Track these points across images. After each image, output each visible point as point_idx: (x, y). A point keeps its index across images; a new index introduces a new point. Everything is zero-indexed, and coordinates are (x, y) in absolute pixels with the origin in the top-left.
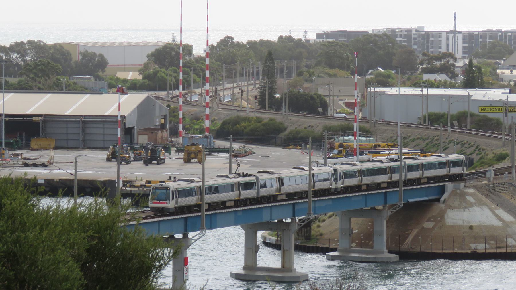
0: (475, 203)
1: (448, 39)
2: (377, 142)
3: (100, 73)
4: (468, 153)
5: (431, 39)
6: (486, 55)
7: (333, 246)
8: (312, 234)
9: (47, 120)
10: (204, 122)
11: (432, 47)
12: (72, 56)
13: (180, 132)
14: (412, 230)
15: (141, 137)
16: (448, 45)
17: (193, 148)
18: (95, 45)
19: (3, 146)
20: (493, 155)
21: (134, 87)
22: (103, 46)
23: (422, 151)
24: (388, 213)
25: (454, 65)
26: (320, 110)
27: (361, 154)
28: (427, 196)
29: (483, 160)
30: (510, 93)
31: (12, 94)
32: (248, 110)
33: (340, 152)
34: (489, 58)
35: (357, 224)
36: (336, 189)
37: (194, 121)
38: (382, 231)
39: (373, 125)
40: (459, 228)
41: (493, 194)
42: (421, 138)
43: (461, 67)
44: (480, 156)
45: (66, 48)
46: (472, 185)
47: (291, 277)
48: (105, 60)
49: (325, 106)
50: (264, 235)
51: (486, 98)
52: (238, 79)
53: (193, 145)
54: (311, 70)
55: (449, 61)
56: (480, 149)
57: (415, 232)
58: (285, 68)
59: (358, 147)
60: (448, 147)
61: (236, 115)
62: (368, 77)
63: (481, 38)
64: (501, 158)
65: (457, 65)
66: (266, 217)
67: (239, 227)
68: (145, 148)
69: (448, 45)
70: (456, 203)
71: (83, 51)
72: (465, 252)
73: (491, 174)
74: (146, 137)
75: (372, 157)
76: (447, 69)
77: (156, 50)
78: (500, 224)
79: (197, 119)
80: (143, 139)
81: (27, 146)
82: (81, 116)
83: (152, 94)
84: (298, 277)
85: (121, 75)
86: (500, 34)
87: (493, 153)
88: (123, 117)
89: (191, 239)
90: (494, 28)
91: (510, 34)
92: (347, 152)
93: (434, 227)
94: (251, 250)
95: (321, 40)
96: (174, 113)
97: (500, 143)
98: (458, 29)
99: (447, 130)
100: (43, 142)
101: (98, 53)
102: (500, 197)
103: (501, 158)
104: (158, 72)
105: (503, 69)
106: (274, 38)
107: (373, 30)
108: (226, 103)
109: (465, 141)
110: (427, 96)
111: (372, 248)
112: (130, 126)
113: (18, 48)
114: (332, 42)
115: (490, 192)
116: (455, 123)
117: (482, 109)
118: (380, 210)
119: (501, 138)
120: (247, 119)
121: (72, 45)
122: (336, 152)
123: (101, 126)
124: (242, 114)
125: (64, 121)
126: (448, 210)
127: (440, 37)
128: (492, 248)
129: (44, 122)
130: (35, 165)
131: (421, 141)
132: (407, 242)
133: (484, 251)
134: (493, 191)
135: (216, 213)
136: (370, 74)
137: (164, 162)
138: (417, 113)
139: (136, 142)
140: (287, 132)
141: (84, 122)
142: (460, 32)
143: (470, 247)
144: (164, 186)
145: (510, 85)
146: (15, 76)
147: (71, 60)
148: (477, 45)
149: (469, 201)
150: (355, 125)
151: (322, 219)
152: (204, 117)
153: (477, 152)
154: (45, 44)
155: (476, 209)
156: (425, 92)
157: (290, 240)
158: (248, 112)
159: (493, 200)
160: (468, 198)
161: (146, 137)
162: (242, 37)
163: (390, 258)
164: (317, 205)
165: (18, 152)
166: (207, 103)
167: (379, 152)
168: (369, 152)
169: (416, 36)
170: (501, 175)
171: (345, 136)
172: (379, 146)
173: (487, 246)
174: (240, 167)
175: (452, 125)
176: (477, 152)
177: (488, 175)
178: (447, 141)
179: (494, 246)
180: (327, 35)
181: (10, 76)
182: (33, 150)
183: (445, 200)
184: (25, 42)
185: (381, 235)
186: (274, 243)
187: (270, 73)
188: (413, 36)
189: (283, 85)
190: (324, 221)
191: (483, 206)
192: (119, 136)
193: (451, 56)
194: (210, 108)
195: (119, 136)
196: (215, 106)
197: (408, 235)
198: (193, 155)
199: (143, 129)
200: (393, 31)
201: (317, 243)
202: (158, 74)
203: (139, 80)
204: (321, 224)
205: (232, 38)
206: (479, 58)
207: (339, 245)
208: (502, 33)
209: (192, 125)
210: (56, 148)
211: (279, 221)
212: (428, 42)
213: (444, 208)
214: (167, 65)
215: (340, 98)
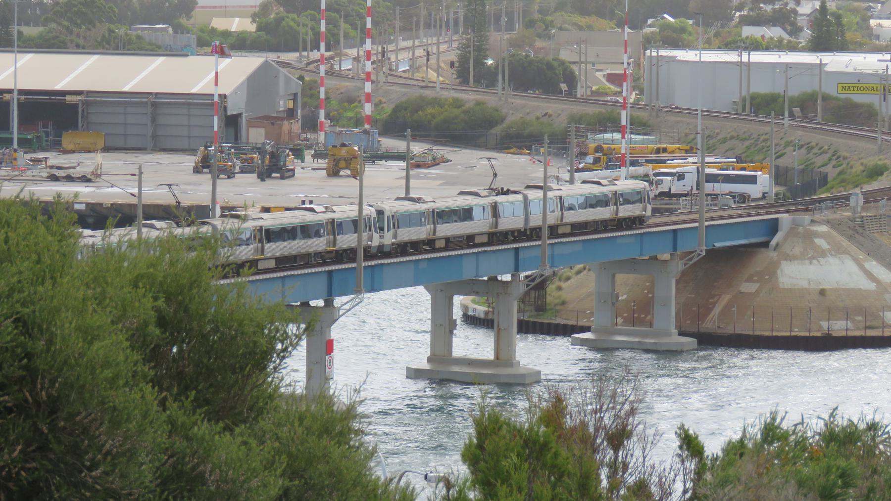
3: (183, 21)
4: (819, 164)
7: (583, 322)
8: (548, 301)
10: (362, 107)
13: (322, 122)
14: (720, 296)
15: (252, 130)
19: (15, 146)
20: (862, 168)
21: (241, 44)
23: (739, 160)
24: (679, 266)
25: (795, 12)
26: (564, 87)
27: (634, 163)
28: (745, 238)
29: (843, 176)
31: (96, 57)
32: (438, 86)
33: (597, 161)
35: (626, 285)
36: (381, 247)
37: (346, 104)
39: (654, 114)
41: (862, 235)
42: (737, 137)
43: (808, 15)
44: (840, 169)
47: (509, 376)
49: (571, 80)
50: (464, 302)
51: (850, 69)
53: (343, 145)
54: (549, 18)
57: (725, 299)
58: (503, 15)
59: (628, 152)
62: (647, 30)
64: (876, 173)
65: (800, 10)
66: (468, 271)
67: (421, 289)
68: (260, 150)
70: (798, 250)
73: (857, 200)
74: (262, 131)
75: (653, 170)
78: (872, 286)
79: (350, 100)
80: (256, 136)
81: (56, 146)
82: (151, 94)
83: (272, 56)
84: (523, 376)
87: (862, 164)
88: (223, 97)
89: (339, 309)
92: (610, 160)
93: (757, 292)
94: (442, 328)
96: (310, 90)
103: (876, 173)
105: (880, 18)
109: (813, 144)
110: (749, 64)
111: (651, 325)
115: (856, 231)
116: (797, 111)
118: (665, 261)
119: (875, 138)
120: (436, 102)
122: (590, 159)
124: (428, 93)
125: (120, 103)
128: (858, 329)
129: (86, 103)
130: (70, 179)
131: (737, 142)
132: (711, 316)
133: (844, 334)
134: (860, 230)
135: (382, 264)
136: (650, 26)
137: (293, 175)
138: (730, 93)
141: (154, 105)
149: (819, 246)
150: (624, 114)
152: (363, 98)
153: (834, 162)
155: (831, 260)
156: (745, 58)
158: (438, 89)
159: (860, 246)
160: (818, 241)
161: (262, 131)
163: (682, 344)
164: (557, 250)
166: (368, 74)
167: (664, 161)
168: (647, 161)
171: (605, 132)
172: (665, 150)
173: (850, 325)
177: (852, 202)
178: (783, 142)
179: (862, 325)
182: (66, 152)
183: (777, 245)
190: (568, 278)
191: (844, 256)
192: (216, 129)
194: (373, 82)
196: (382, 78)
197: (714, 304)
201: (556, 316)
203: (250, 32)
204: (564, 285)
207: (593, 322)
209: (341, 111)
210: (106, 149)
211: (490, 279)
213: (775, 259)
215: (598, 66)
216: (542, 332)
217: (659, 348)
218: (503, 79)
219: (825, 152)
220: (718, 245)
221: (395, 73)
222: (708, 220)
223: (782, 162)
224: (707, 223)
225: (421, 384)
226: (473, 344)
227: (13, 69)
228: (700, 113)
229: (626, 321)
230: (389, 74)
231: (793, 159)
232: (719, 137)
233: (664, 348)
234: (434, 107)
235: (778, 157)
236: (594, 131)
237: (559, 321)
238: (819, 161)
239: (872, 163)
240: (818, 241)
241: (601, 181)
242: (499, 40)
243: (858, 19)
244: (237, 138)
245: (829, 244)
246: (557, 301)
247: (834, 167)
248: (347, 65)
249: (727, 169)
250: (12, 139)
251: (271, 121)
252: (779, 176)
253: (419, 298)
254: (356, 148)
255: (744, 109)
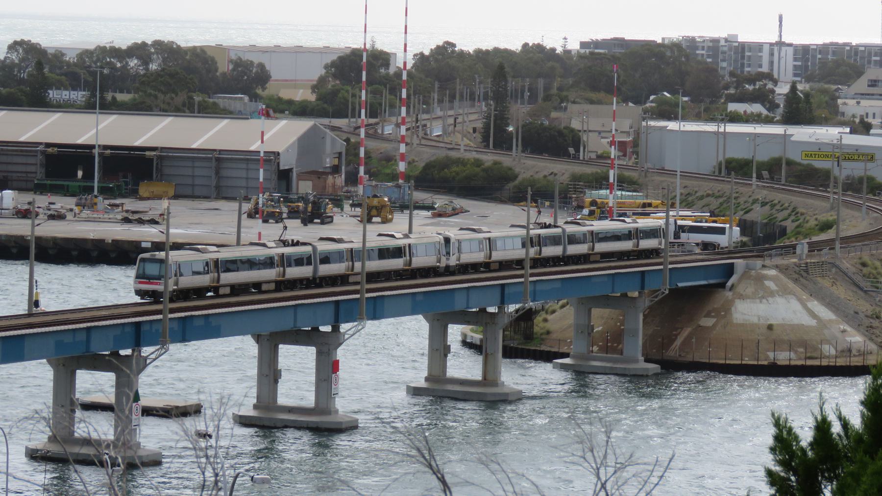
0: (777, 292)
1: (772, 54)
2: (647, 199)
3: (259, 91)
4: (780, 219)
5: (747, 54)
6: (827, 78)
7: (564, 350)
8: (535, 331)
9: (223, 158)
10: (398, 165)
11: (749, 66)
12: (218, 65)
13: (361, 177)
14: (682, 329)
15: (301, 183)
16: (771, 63)
17: (375, 202)
18: (253, 49)
19: (96, 193)
20: (816, 223)
21: (300, 110)
22: (265, 51)
23: (713, 214)
24: (646, 303)
25: (773, 91)
26: (571, 150)
29: (799, 229)
30: (851, 133)
32: (462, 148)
33: (592, 213)
34: (829, 82)
35: (601, 318)
36: (447, 267)
37: (384, 162)
38: (637, 330)
39: (643, 174)
40: (753, 327)
41: (806, 279)
42: (713, 195)
43: (785, 95)
44: (797, 223)
45: (210, 53)
46: (775, 264)
47: (494, 394)
48: (267, 71)
49: (576, 142)
51: (813, 140)
52: (456, 103)
53: (375, 196)
54: (565, 93)
55: (765, 85)
56: (797, 213)
60: (751, 210)
61: (444, 155)
62: (648, 105)
63: (820, 54)
64: (825, 227)
66: (459, 304)
68: (304, 199)
69: (771, 63)
71: (234, 57)
72: (760, 363)
73: (803, 248)
76: (763, 97)
77: (340, 58)
78: (813, 323)
79: (389, 159)
81: (133, 193)
84: (507, 394)
85: (286, 94)
86: (848, 48)
87: (816, 219)
89: (345, 333)
90: (841, 40)
91: (863, 49)
92: (602, 211)
93: (714, 325)
94: (439, 350)
95: (588, 51)
96: (352, 149)
97: (825, 205)
98: (786, 39)
99: (751, 185)
100: (157, 188)
101: (256, 61)
102: (815, 283)
103: (825, 227)
104: (338, 91)
105: (846, 98)
106: (515, 46)
107: (663, 39)
108: (436, 138)
109: (776, 202)
110: (725, 134)
111: (622, 354)
112: (286, 168)
113: (139, 50)
114: (605, 54)
115: (802, 275)
116: (765, 174)
117: (807, 155)
118: (492, 314)
119: (828, 198)
121: (220, 49)
122: (586, 211)
123: (189, 164)
124: (454, 154)
126: (737, 302)
127: (761, 50)
128: (800, 359)
129: (161, 158)
130: (141, 222)
131: (712, 199)
132: (674, 346)
133: (787, 363)
134: (805, 274)
136: (652, 102)
137: (332, 221)
139: (294, 190)
140: (516, 182)
141: (218, 160)
142: (790, 45)
143: (768, 357)
144: (157, 257)
145: (854, 122)
146: (129, 92)
147: (216, 70)
148: (813, 64)
149: (769, 288)
150: (611, 173)
151: (551, 309)
152: (398, 158)
153: (793, 218)
154: (179, 46)
156: (722, 130)
157: (496, 339)
158: (462, 151)
159: (804, 287)
160: (767, 283)
161: (310, 183)
162: (467, 44)
163: (647, 369)
164: (539, 287)
165: (118, 201)
166: (403, 137)
169: (725, 49)
170: (818, 250)
171: (601, 188)
172: (650, 205)
173: (793, 355)
174: (287, 232)
175: (760, 177)
176: (793, 218)
177: (798, 251)
178: (751, 200)
179: (803, 356)
180: (596, 44)
181: (121, 92)
182: (142, 199)
183: (733, 285)
184: (150, 43)
185: (635, 334)
186: (478, 343)
187: (500, 97)
188: (721, 49)
189: (519, 113)
190: (554, 312)
191: (790, 296)
192: (261, 180)
193: (769, 76)
194: (407, 144)
195: (261, 180)
196: (416, 141)
197: (676, 336)
198: (374, 212)
199: (306, 173)
200: (693, 40)
201: (541, 344)
202: (340, 95)
203: (310, 102)
204: (549, 317)
205: (454, 45)
206: (813, 81)
207: (572, 350)
208: (851, 47)
210: (176, 197)
212: (743, 57)
213: (730, 298)
214: (355, 81)
215: (603, 135)
216: (522, 357)
217: (627, 373)
218: (517, 145)
219: (786, 209)
220: (680, 285)
221: (429, 137)
222: (671, 263)
223: (749, 217)
224: (670, 266)
225: (424, 400)
226: (464, 366)
227: (99, 128)
228: (679, 173)
229: (601, 349)
230: (423, 138)
231: (758, 214)
232: (698, 194)
233: (634, 373)
234: (458, 166)
235: (746, 213)
236: (592, 187)
237: (544, 348)
238: (781, 216)
239: (824, 219)
240: (767, 283)
241: (395, 234)
242: (519, 113)
243: (827, 98)
244: (288, 189)
245: (776, 285)
246: (542, 331)
247: (793, 221)
248: (388, 130)
249: (701, 222)
250: (93, 187)
251: (317, 175)
252: (746, 227)
253: (242, 349)
254: (386, 199)
255: (720, 172)
